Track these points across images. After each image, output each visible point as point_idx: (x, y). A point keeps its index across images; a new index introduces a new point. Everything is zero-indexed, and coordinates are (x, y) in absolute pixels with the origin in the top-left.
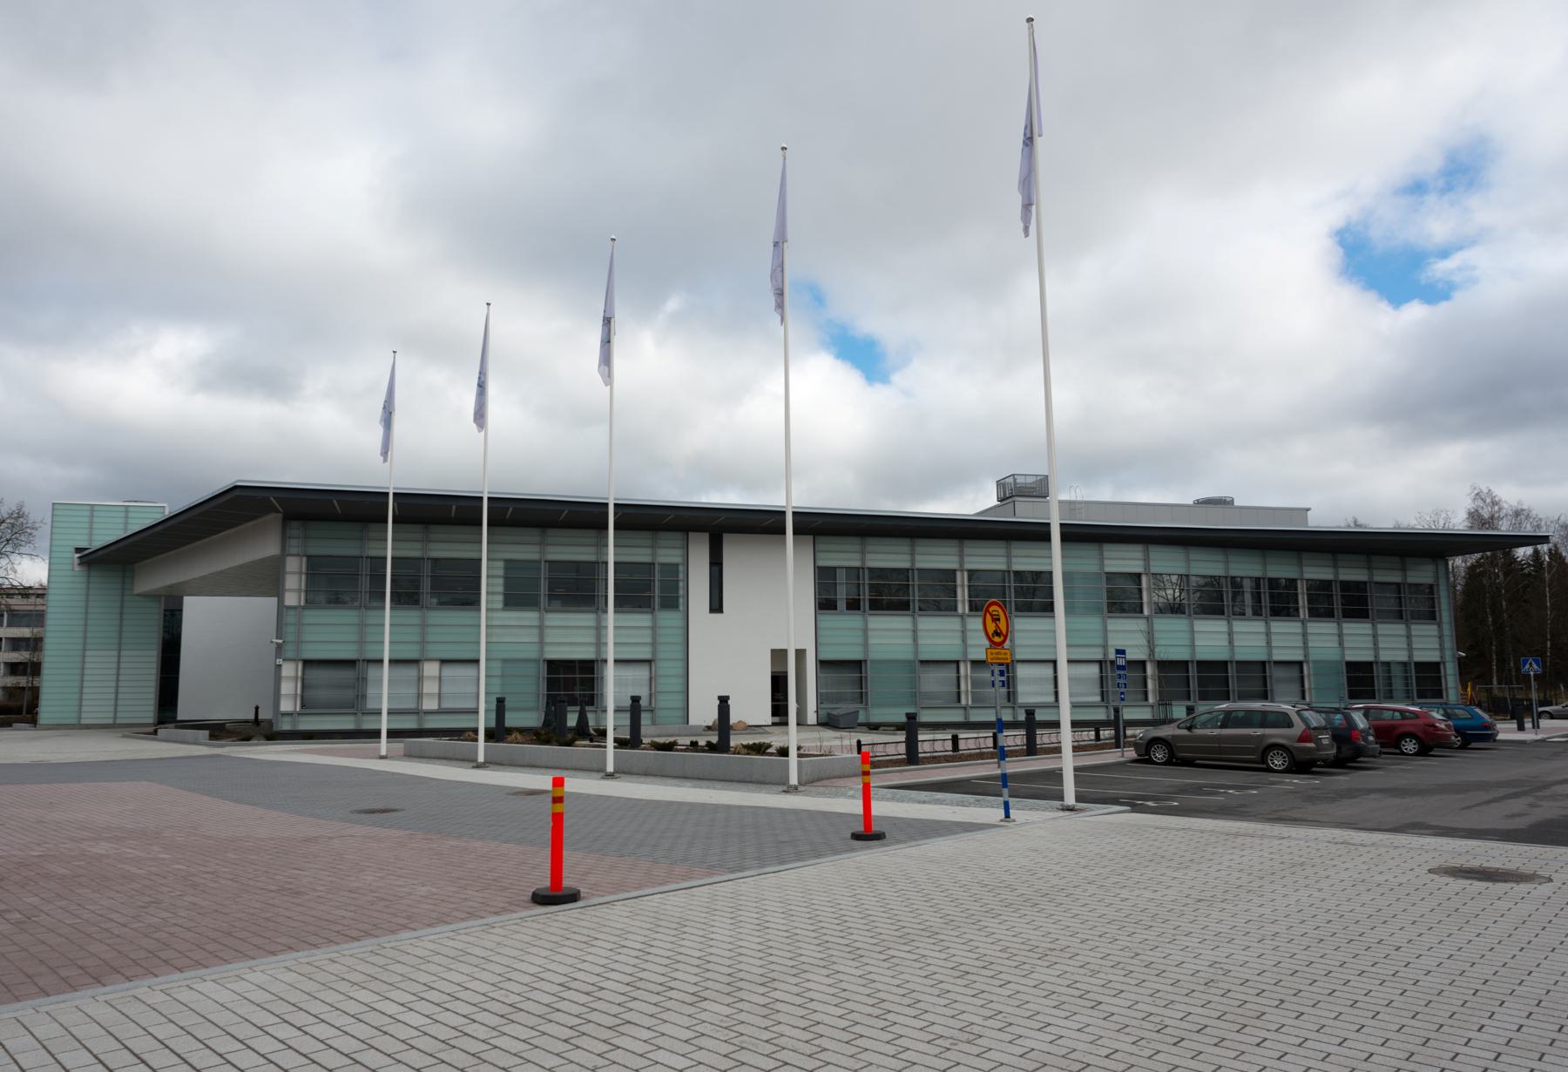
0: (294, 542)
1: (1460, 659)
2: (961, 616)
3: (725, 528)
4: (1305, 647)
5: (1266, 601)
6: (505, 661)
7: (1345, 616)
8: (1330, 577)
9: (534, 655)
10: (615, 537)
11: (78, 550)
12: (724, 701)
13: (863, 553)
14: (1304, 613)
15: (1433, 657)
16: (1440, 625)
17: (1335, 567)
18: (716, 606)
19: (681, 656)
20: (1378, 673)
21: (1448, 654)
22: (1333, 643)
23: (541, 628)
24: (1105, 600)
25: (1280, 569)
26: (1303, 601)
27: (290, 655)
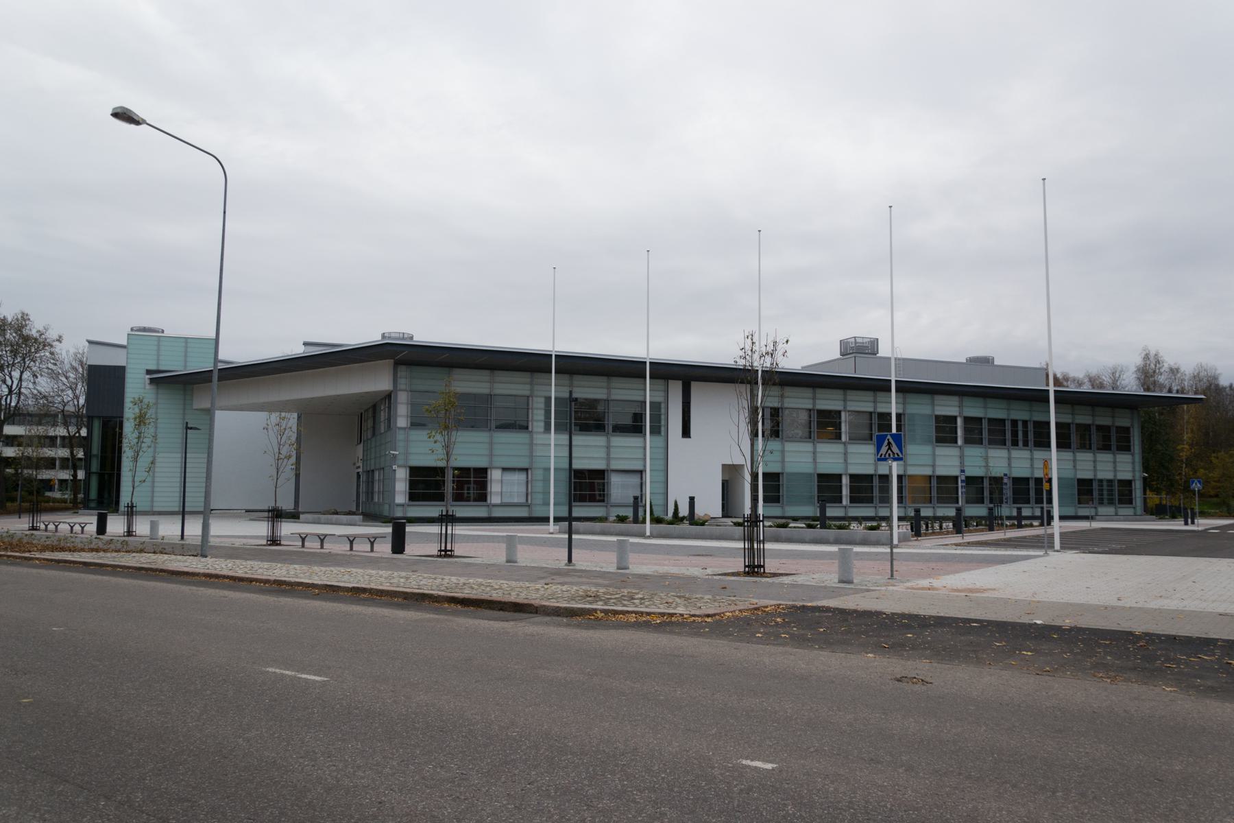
1: (1145, 479)
2: (845, 443)
3: (687, 377)
5: (1031, 436)
7: (990, 443)
8: (1090, 422)
10: (1056, 408)
11: (149, 372)
12: (692, 499)
15: (1128, 476)
16: (1133, 455)
17: (985, 407)
18: (686, 433)
19: (662, 468)
20: (1095, 485)
21: (1138, 475)
24: (934, 434)
27: (401, 462)
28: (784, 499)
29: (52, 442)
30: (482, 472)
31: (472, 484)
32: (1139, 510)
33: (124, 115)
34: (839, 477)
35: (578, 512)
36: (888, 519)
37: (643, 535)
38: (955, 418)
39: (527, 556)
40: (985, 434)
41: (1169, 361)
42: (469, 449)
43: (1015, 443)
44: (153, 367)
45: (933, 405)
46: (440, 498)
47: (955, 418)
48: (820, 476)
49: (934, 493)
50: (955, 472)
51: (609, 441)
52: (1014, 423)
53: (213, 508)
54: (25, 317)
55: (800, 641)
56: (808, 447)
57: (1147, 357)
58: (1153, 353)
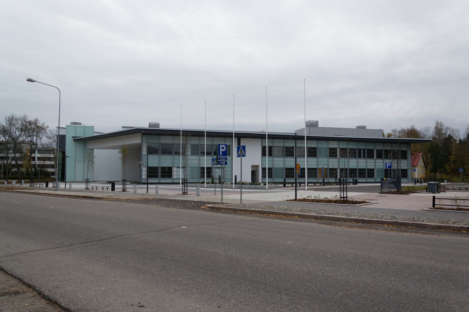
0: (144, 140)
4: (375, 165)
6: (191, 167)
9: (198, 166)
11: (73, 137)
13: (284, 143)
14: (375, 157)
15: (406, 168)
17: (357, 145)
21: (409, 167)
22: (356, 164)
23: (199, 160)
25: (370, 147)
26: (375, 154)
28: (273, 176)
29: (49, 159)
30: (170, 169)
31: (167, 172)
32: (410, 180)
33: (30, 80)
34: (336, 169)
35: (287, 181)
36: (304, 183)
37: (204, 187)
38: (336, 148)
39: (139, 191)
40: (348, 154)
41: (446, 125)
42: (164, 161)
43: (360, 157)
44: (74, 136)
45: (328, 144)
46: (157, 176)
47: (336, 148)
48: (286, 169)
49: (328, 174)
50: (336, 167)
51: (200, 158)
52: (360, 150)
53: (91, 179)
54: (36, 120)
55: (210, 211)
56: (282, 159)
57: (438, 123)
58: (439, 122)
